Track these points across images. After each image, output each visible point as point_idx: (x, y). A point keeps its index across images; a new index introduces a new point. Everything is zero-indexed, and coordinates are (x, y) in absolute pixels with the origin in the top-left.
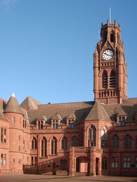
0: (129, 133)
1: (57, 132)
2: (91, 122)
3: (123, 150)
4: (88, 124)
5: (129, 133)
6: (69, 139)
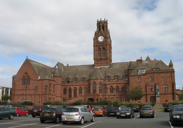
0: (112, 85)
1: (77, 85)
3: (110, 94)
4: (92, 81)
5: (112, 85)
6: (83, 89)
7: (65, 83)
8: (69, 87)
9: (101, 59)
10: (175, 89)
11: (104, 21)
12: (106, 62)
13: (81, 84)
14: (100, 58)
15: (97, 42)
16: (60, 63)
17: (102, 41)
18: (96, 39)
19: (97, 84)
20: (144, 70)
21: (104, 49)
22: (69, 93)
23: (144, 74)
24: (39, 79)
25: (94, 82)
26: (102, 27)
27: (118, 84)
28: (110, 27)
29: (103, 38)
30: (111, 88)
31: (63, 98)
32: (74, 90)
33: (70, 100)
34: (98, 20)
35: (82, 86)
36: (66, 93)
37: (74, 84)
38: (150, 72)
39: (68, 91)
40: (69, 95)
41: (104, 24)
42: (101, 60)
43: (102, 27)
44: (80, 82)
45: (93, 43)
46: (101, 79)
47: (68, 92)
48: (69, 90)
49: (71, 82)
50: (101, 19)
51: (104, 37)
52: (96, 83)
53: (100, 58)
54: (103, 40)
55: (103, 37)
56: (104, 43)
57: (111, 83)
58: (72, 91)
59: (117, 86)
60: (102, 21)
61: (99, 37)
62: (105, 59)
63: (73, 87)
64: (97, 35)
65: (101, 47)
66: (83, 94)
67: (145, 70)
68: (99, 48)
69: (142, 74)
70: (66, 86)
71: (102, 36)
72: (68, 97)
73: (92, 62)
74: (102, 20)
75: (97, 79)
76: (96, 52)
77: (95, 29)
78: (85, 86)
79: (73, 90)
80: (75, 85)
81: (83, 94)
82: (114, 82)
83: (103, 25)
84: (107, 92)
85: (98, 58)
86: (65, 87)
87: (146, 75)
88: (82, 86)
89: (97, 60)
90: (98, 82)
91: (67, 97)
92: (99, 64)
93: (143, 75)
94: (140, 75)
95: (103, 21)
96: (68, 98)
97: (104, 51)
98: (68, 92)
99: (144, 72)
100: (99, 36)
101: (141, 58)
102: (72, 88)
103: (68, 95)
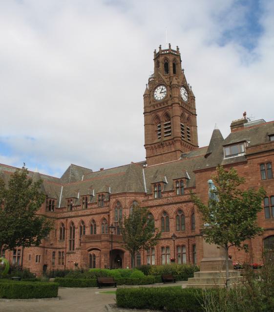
1: (85, 214)
2: (117, 196)
6: (98, 223)
7: (64, 210)
8: (69, 220)
9: (162, 144)
10: (134, 168)
11: (170, 49)
12: (173, 150)
13: (94, 211)
14: (159, 140)
15: (153, 103)
16: (78, 168)
17: (166, 97)
18: (149, 96)
19: (123, 207)
20: (243, 147)
21: (167, 116)
22: (71, 238)
23: (239, 161)
24: (59, 207)
25: (118, 202)
26: (168, 64)
27: (180, 205)
28: (186, 65)
29: (165, 90)
30: (180, 215)
31: (57, 251)
32: (81, 227)
33: (71, 255)
34: (155, 52)
35: (96, 217)
36: (64, 238)
37: (80, 213)
38: (258, 150)
39: (68, 232)
40: (70, 241)
41: (168, 57)
42: (161, 145)
43: (168, 64)
44: (93, 206)
45: (143, 106)
46: (136, 193)
47: (68, 233)
48: (61, 229)
49: (76, 206)
50: (170, 46)
51: (166, 87)
52: (121, 206)
53: (159, 140)
54: (164, 96)
55: (164, 88)
56: (167, 102)
57: (164, 201)
58: (76, 230)
59: (180, 210)
60: (164, 51)
61: (156, 90)
62: (170, 142)
63: (79, 219)
64: (153, 84)
65: (160, 114)
66: (173, 230)
67: (243, 147)
68: (157, 117)
69: (232, 162)
70: (63, 218)
71: (161, 87)
72: (68, 247)
73: (139, 154)
74: (172, 48)
75: (125, 193)
76: (150, 127)
77: (149, 69)
78: (102, 216)
79: (77, 228)
80: (83, 214)
81: (173, 230)
82: (171, 200)
83: (166, 59)
84: (104, 236)
85: (157, 141)
86: (62, 220)
87: (245, 163)
88: (96, 216)
89: (152, 147)
90: (128, 201)
91: (66, 248)
92: (157, 157)
93: (243, 162)
94: (227, 163)
95: (166, 50)
96: (68, 250)
97: (169, 122)
98: (68, 233)
99: (243, 154)
100: (156, 88)
101: (245, 115)
102: (77, 221)
103: (68, 243)
